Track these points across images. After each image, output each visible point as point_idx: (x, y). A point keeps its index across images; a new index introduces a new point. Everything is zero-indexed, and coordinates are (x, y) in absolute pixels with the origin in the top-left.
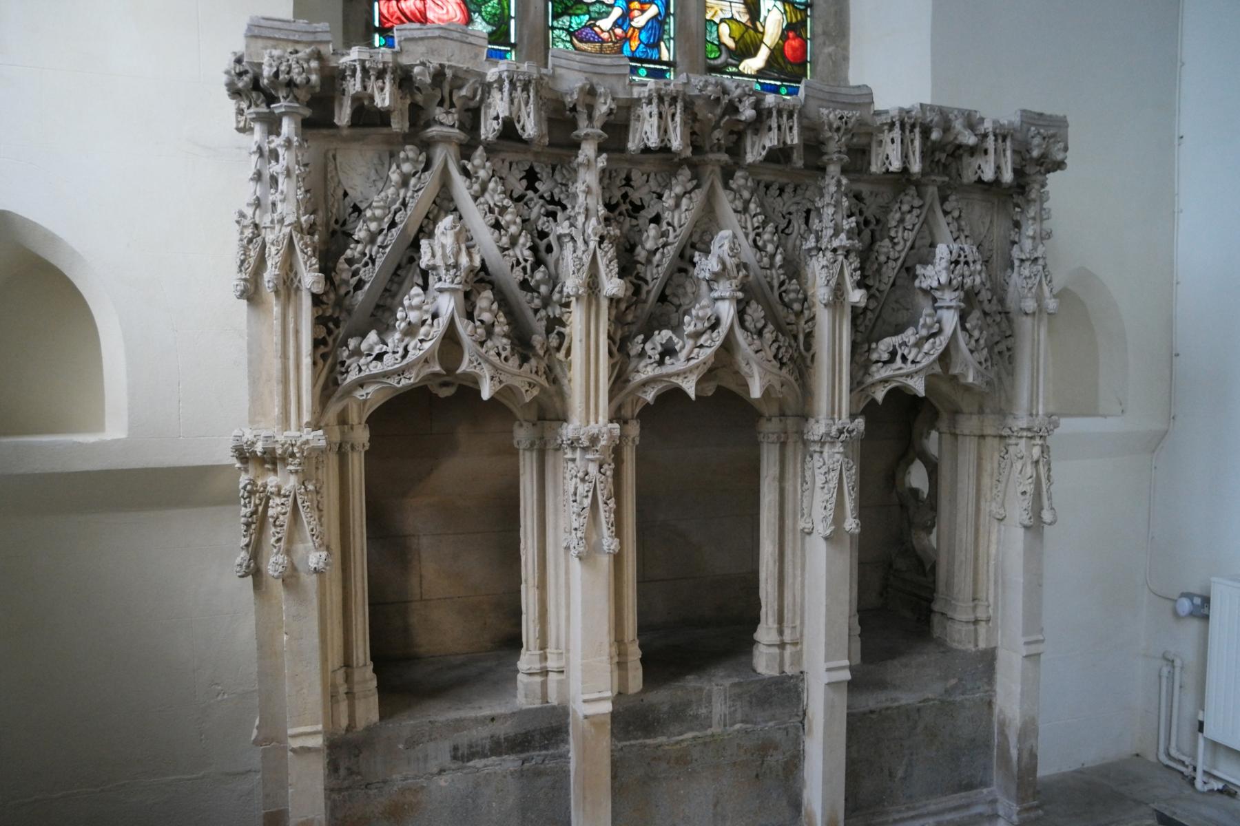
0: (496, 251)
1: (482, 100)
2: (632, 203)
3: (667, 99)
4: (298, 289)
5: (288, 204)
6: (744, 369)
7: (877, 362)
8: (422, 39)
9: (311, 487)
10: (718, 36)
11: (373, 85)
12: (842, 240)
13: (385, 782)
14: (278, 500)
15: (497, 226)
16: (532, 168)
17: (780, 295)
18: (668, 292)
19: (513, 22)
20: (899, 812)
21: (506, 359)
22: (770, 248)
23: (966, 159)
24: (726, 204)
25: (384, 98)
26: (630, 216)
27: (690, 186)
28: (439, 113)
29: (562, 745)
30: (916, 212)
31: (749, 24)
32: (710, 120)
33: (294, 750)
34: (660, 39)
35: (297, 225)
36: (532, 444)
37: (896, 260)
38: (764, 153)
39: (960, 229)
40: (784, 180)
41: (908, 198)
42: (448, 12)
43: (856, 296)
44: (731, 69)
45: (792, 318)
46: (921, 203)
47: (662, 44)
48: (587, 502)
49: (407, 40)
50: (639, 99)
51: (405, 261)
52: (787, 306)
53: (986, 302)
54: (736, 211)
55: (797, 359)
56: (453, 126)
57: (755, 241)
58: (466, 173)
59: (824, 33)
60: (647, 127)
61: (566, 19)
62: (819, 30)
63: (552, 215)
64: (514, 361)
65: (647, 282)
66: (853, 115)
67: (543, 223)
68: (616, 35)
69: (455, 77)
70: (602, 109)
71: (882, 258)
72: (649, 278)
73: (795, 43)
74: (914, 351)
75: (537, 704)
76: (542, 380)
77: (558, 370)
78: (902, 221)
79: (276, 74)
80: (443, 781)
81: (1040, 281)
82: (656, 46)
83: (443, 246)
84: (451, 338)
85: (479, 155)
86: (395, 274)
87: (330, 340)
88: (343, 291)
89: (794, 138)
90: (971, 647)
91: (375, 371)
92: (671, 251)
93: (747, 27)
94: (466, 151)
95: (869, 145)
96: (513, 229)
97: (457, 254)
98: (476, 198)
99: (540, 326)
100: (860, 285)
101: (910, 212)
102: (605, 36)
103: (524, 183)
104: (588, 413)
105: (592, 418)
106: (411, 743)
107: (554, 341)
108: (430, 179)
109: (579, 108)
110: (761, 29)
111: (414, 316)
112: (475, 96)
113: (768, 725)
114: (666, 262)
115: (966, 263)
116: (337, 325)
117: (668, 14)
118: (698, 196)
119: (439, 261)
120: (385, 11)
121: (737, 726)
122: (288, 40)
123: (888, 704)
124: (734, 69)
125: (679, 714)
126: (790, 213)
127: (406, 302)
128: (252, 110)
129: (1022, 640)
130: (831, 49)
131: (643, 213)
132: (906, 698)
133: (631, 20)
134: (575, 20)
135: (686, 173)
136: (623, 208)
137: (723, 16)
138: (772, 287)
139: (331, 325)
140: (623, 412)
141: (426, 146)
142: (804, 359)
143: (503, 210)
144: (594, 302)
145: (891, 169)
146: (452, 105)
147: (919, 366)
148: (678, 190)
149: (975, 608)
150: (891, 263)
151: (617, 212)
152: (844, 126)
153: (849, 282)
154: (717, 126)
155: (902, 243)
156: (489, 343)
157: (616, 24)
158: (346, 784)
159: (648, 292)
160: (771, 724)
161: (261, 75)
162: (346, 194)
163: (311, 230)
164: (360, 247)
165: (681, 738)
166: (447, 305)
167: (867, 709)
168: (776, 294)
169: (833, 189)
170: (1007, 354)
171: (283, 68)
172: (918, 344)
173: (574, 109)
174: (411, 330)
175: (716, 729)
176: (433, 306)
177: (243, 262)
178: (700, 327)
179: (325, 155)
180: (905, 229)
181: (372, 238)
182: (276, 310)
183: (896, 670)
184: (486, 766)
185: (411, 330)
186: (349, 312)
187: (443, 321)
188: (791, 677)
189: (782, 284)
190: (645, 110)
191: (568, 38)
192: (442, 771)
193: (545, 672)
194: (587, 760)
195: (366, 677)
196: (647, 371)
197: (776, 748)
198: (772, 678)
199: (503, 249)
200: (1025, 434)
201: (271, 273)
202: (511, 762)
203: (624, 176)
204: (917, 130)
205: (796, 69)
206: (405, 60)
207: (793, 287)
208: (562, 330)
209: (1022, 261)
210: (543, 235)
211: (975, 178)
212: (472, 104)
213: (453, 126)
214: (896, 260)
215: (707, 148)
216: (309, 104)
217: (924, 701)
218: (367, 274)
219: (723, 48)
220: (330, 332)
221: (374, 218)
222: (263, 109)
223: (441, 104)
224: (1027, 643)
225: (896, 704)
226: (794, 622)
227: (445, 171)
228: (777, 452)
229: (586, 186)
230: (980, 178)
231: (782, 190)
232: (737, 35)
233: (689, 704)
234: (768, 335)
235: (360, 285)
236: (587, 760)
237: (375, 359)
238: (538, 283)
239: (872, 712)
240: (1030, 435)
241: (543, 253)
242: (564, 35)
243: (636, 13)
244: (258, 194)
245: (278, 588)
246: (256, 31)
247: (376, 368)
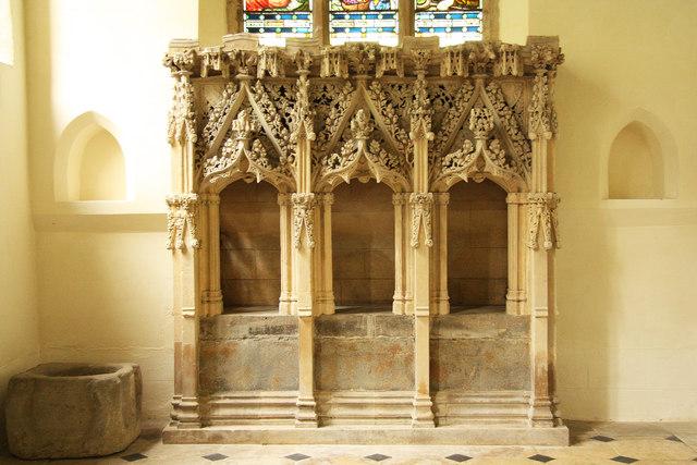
5: (184, 109)
11: (213, 61)
12: (420, 111)
15: (266, 112)
25: (217, 67)
28: (240, 70)
39: (497, 99)
45: (402, 146)
52: (400, 141)
55: (404, 166)
64: (269, 167)
67: (287, 110)
75: (286, 314)
80: (246, 342)
84: (243, 157)
90: (515, 314)
94: (253, 83)
96: (272, 113)
97: (244, 126)
106: (232, 324)
107: (290, 159)
111: (229, 150)
113: (395, 337)
114: (340, 124)
115: (485, 117)
118: (355, 94)
125: (351, 327)
132: (474, 335)
141: (237, 83)
143: (268, 106)
163: (193, 118)
166: (241, 146)
174: (228, 156)
176: (236, 147)
181: (217, 120)
185: (228, 156)
187: (239, 152)
192: (244, 338)
195: (217, 295)
201: (178, 134)
206: (225, 50)
218: (215, 134)
227: (245, 90)
229: (302, 95)
231: (400, 87)
233: (355, 323)
234: (382, 155)
235: (212, 138)
245: (179, 252)
247: (216, 170)
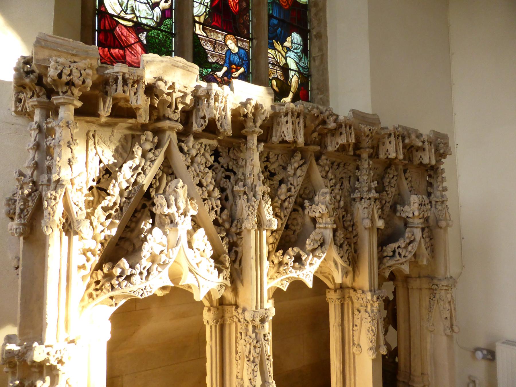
7: (387, 256)
24: (317, 174)
27: (301, 162)
30: (395, 178)
37: (389, 202)
38: (337, 147)
41: (392, 171)
43: (380, 224)
50: (280, 113)
51: (140, 207)
54: (322, 177)
56: (177, 121)
58: (181, 150)
59: (318, 89)
60: (284, 129)
63: (228, 177)
66: (375, 128)
74: (404, 251)
78: (390, 182)
79: (60, 75)
86: (133, 215)
92: (293, 199)
101: (393, 178)
110: (289, 84)
118: (305, 168)
128: (35, 99)
130: (321, 96)
137: (273, 76)
145: (390, 157)
148: (296, 165)
153: (376, 216)
154: (314, 131)
157: (224, 75)
161: (46, 75)
171: (65, 71)
172: (406, 247)
180: (391, 187)
189: (343, 217)
190: (284, 119)
200: (445, 288)
203: (266, 155)
204: (400, 138)
209: (437, 202)
211: (418, 162)
213: (177, 121)
222: (44, 99)
230: (421, 163)
234: (345, 247)
237: (125, 279)
238: (224, 221)
240: (447, 288)
244: (36, 159)
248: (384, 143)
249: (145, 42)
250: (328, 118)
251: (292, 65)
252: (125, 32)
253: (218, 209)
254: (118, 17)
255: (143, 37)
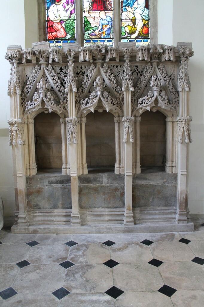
0: (53, 84)
1: (49, 55)
2: (82, 72)
3: (85, 51)
4: (17, 94)
6: (104, 106)
7: (139, 104)
8: (37, 45)
9: (19, 129)
10: (125, 30)
11: (28, 55)
12: (127, 77)
13: (36, 186)
14: (14, 131)
15: (53, 79)
16: (61, 67)
17: (115, 90)
18: (90, 90)
19: (76, 34)
20: (149, 208)
21: (53, 105)
22: (113, 80)
23: (163, 55)
26: (82, 75)
27: (93, 68)
29: (70, 183)
30: (150, 69)
31: (133, 26)
32: (96, 54)
33: (18, 176)
34: (110, 33)
35: (16, 82)
36: (63, 122)
37: (145, 80)
38: (109, 59)
39: (163, 72)
40: (117, 64)
42: (62, 34)
44: (128, 38)
45: (118, 95)
46: (152, 67)
47: (111, 34)
48: (70, 133)
49: (34, 46)
50: (80, 51)
52: (118, 92)
53: (171, 89)
54: (104, 72)
56: (44, 61)
57: (109, 78)
59: (152, 26)
61: (88, 31)
62: (151, 25)
64: (55, 106)
65: (84, 89)
67: (64, 78)
68: (99, 34)
69: (43, 52)
70: (72, 54)
71: (141, 80)
72: (85, 88)
73: (145, 29)
74: (147, 101)
75: (65, 174)
76: (62, 109)
77: (66, 107)
79: (11, 56)
81: (184, 83)
82: (109, 34)
83: (40, 84)
85: (50, 66)
87: (23, 103)
88: (25, 94)
89: (114, 56)
91: (30, 108)
93: (133, 27)
95: (136, 55)
98: (49, 74)
99: (62, 98)
100: (133, 86)
102: (97, 34)
103: (60, 70)
104: (72, 116)
105: (72, 116)
106: (41, 179)
107: (65, 101)
108: (41, 72)
109: (68, 55)
110: (136, 27)
111: (35, 97)
112: (47, 55)
114: (88, 84)
115: (159, 80)
116: (25, 100)
117: (112, 27)
118: (95, 70)
119: (40, 87)
120: (49, 36)
121: (109, 184)
122: (14, 49)
123: (147, 183)
124: (129, 38)
125: (95, 180)
126: (119, 72)
127: (34, 95)
129: (180, 171)
131: (85, 74)
132: (152, 183)
133: (103, 29)
134: (90, 31)
135: (93, 65)
136: (80, 73)
138: (113, 88)
139: (23, 100)
140: (82, 116)
142: (122, 104)
143: (54, 76)
144: (71, 93)
146: (43, 57)
147: (148, 104)
149: (172, 163)
150: (144, 81)
151: (79, 75)
152: (128, 52)
155: (146, 76)
156: (49, 102)
158: (29, 185)
159: (85, 90)
160: (117, 185)
162: (27, 76)
164: (28, 85)
165: (96, 185)
167: (142, 184)
168: (114, 89)
169: (126, 65)
170: (177, 102)
173: (67, 55)
175: (104, 184)
177: (8, 90)
178: (93, 97)
179: (23, 69)
182: (13, 97)
183: (149, 176)
184: (55, 186)
185: (35, 100)
186: (27, 98)
188: (122, 175)
191: (88, 36)
192: (46, 186)
193: (67, 168)
194: (75, 185)
196: (84, 107)
197: (118, 190)
198: (117, 174)
199: (54, 84)
200: (180, 120)
202: (59, 186)
205: (146, 35)
206: (34, 50)
207: (118, 88)
208: (67, 99)
210: (64, 80)
212: (47, 56)
213: (44, 61)
214: (145, 80)
215: (97, 59)
216: (18, 60)
217: (157, 184)
218: (30, 90)
219: (126, 33)
220: (23, 101)
221: (31, 80)
223: (41, 57)
224: (181, 171)
225: (149, 184)
226: (122, 162)
228: (118, 124)
231: (117, 67)
232: (130, 29)
233: (97, 178)
235: (28, 92)
236: (75, 185)
239: (143, 185)
241: (64, 84)
242: (87, 35)
243: (104, 28)
246: (9, 48)
247: (30, 107)
248: (138, 54)
249: (64, 27)
250: (102, 49)
251: (138, 16)
252: (57, 25)
253: (60, 87)
254: (54, 20)
255: (63, 25)
